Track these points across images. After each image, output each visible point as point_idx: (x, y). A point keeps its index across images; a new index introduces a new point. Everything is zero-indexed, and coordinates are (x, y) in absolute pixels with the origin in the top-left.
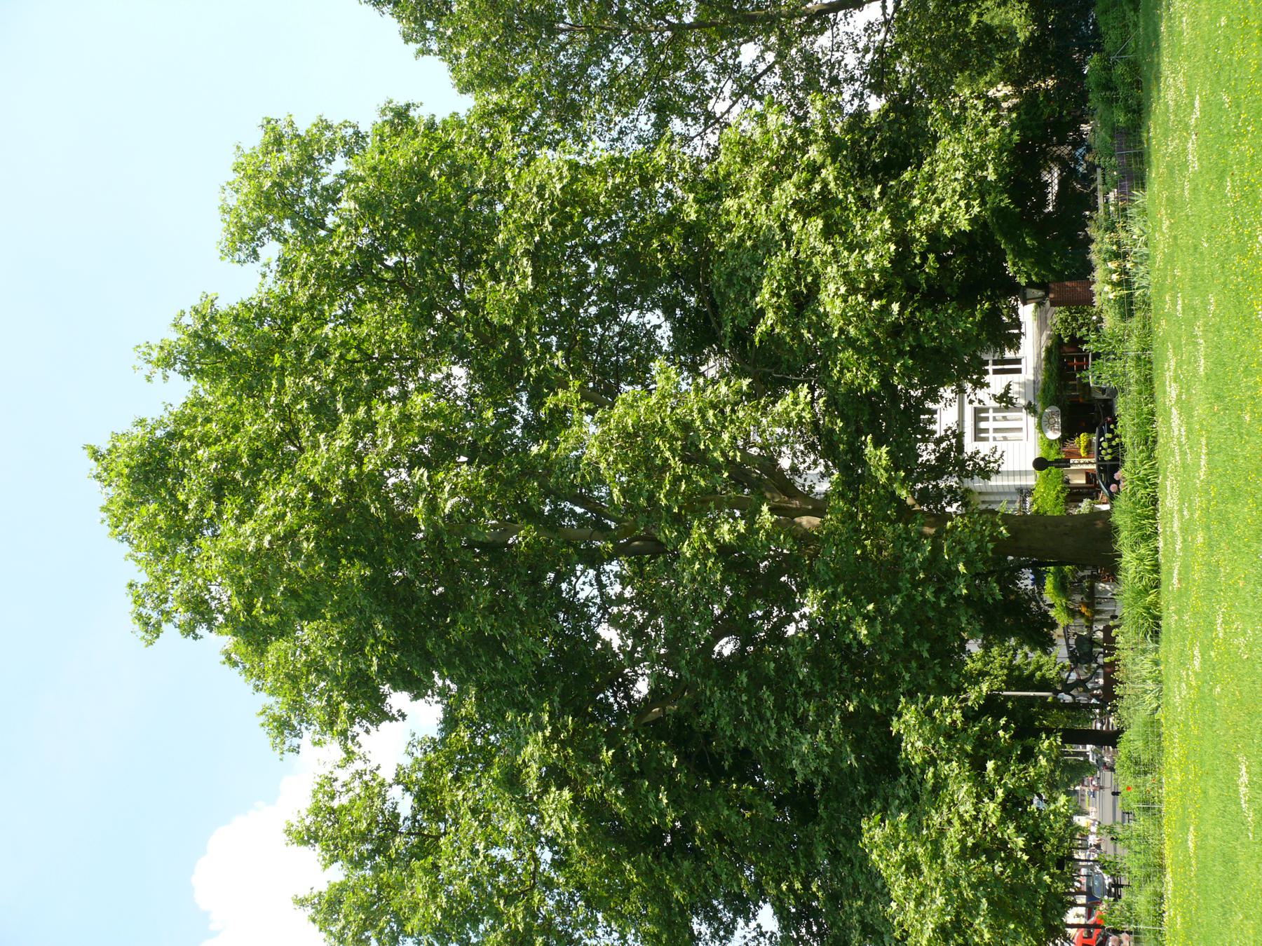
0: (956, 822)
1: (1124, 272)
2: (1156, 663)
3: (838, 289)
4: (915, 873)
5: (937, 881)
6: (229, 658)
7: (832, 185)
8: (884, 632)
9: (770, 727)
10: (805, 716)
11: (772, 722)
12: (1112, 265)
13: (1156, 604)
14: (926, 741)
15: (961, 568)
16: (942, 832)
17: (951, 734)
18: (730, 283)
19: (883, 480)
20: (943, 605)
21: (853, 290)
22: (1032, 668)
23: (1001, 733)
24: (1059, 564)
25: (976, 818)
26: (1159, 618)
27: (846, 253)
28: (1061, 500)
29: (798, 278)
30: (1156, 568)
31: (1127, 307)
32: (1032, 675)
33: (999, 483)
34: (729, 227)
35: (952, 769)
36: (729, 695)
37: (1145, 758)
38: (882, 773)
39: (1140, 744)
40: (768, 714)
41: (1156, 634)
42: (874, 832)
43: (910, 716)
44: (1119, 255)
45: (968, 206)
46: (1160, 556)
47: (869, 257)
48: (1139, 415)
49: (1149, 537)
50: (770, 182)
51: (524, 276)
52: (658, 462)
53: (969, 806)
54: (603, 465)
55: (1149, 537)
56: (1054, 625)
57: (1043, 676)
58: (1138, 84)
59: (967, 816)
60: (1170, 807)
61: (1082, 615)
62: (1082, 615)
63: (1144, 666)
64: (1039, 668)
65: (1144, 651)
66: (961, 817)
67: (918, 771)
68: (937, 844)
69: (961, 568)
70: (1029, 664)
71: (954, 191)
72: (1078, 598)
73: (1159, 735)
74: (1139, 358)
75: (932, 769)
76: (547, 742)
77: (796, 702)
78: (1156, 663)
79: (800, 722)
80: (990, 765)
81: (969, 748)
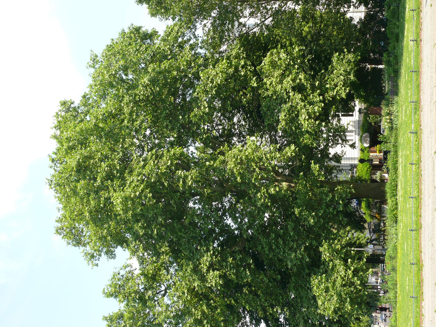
0: (339, 278)
1: (391, 119)
2: (396, 230)
3: (305, 117)
4: (326, 296)
5: (335, 293)
6: (57, 232)
7: (303, 81)
8: (318, 221)
9: (281, 251)
10: (292, 247)
11: (282, 249)
12: (388, 117)
13: (396, 214)
14: (330, 254)
15: (341, 202)
16: (335, 281)
17: (337, 251)
18: (268, 110)
19: (316, 174)
20: (335, 213)
21: (310, 117)
22: (355, 239)
23: (352, 252)
24: (367, 197)
25: (345, 276)
26: (397, 217)
27: (308, 106)
28: (369, 171)
29: (292, 111)
30: (397, 204)
31: (391, 129)
32: (356, 242)
33: (345, 162)
34: (267, 90)
35: (337, 262)
36: (268, 241)
37: (393, 256)
38: (316, 264)
39: (391, 252)
40: (281, 246)
41: (396, 222)
42: (315, 281)
43: (326, 246)
44: (389, 114)
45: (345, 89)
46: (398, 201)
47: (316, 108)
48: (393, 161)
49: (395, 195)
50: (283, 76)
51: (205, 108)
52: (252, 169)
53: (343, 272)
54: (235, 170)
55: (395, 195)
56: (365, 221)
57: (360, 242)
58: (397, 63)
59: (342, 275)
60: (399, 269)
61: (376, 218)
62: (376, 218)
63: (393, 231)
64: (359, 239)
65: (393, 227)
66: (341, 276)
67: (327, 263)
68: (334, 284)
69: (341, 202)
70: (354, 238)
71: (341, 84)
72: (375, 211)
73: (397, 249)
74: (394, 145)
75: (331, 262)
76: (211, 256)
77: (289, 243)
78: (396, 230)
79: (291, 249)
80: (349, 260)
81: (343, 256)
